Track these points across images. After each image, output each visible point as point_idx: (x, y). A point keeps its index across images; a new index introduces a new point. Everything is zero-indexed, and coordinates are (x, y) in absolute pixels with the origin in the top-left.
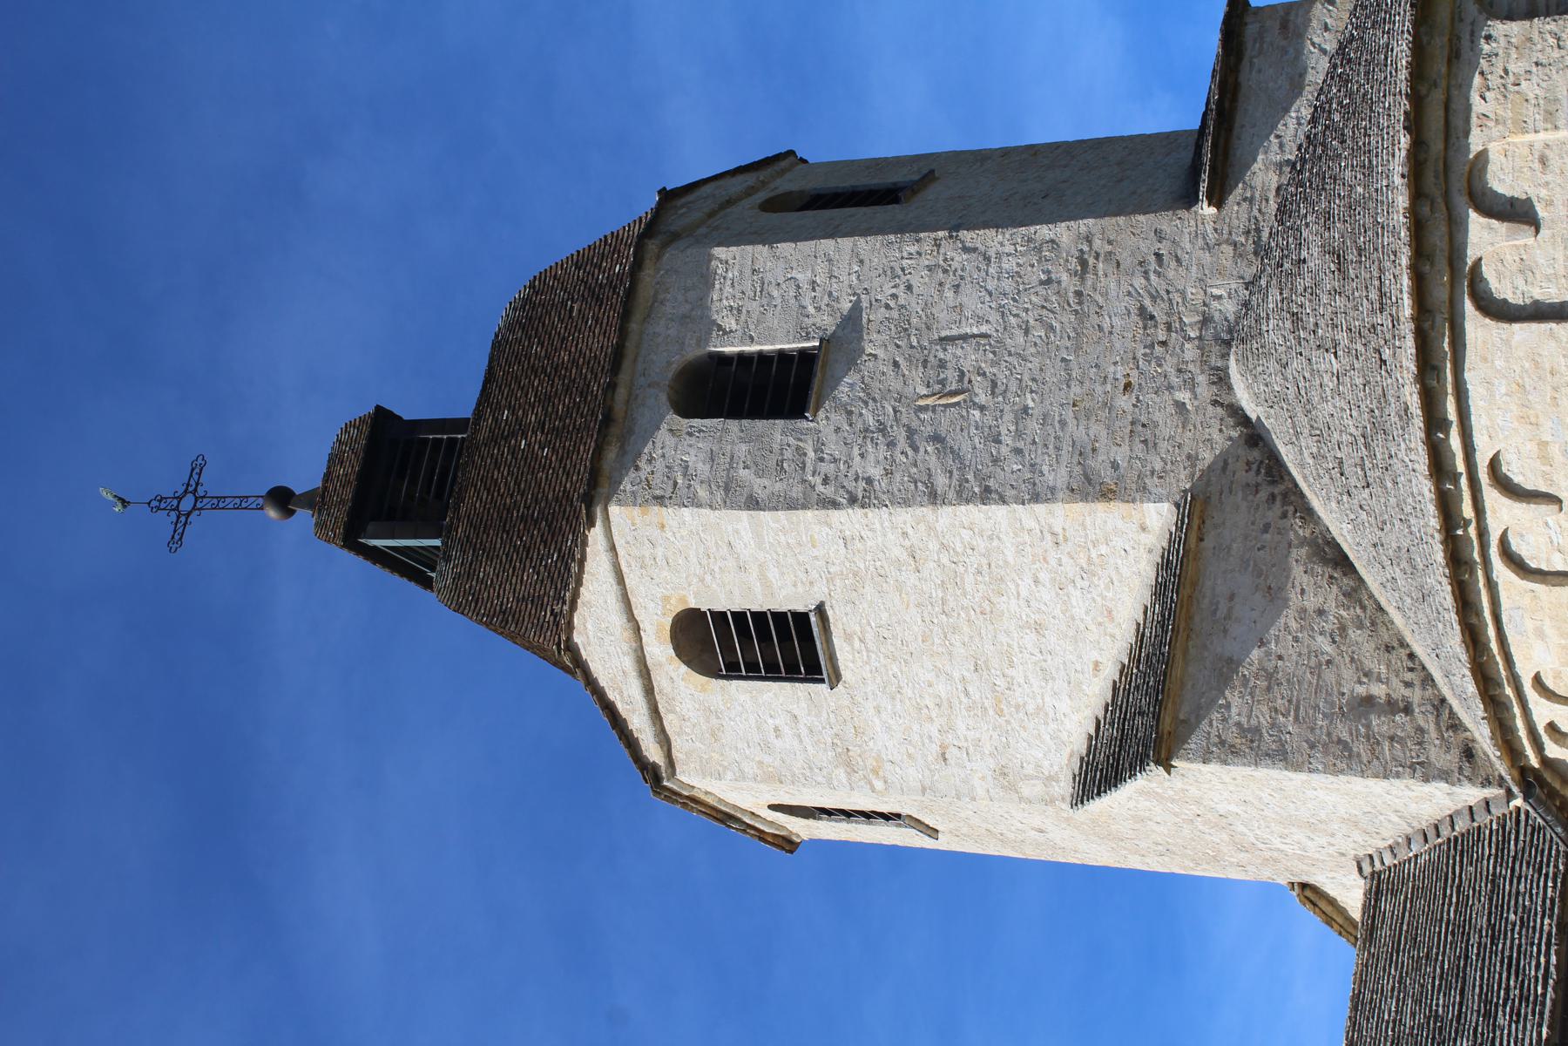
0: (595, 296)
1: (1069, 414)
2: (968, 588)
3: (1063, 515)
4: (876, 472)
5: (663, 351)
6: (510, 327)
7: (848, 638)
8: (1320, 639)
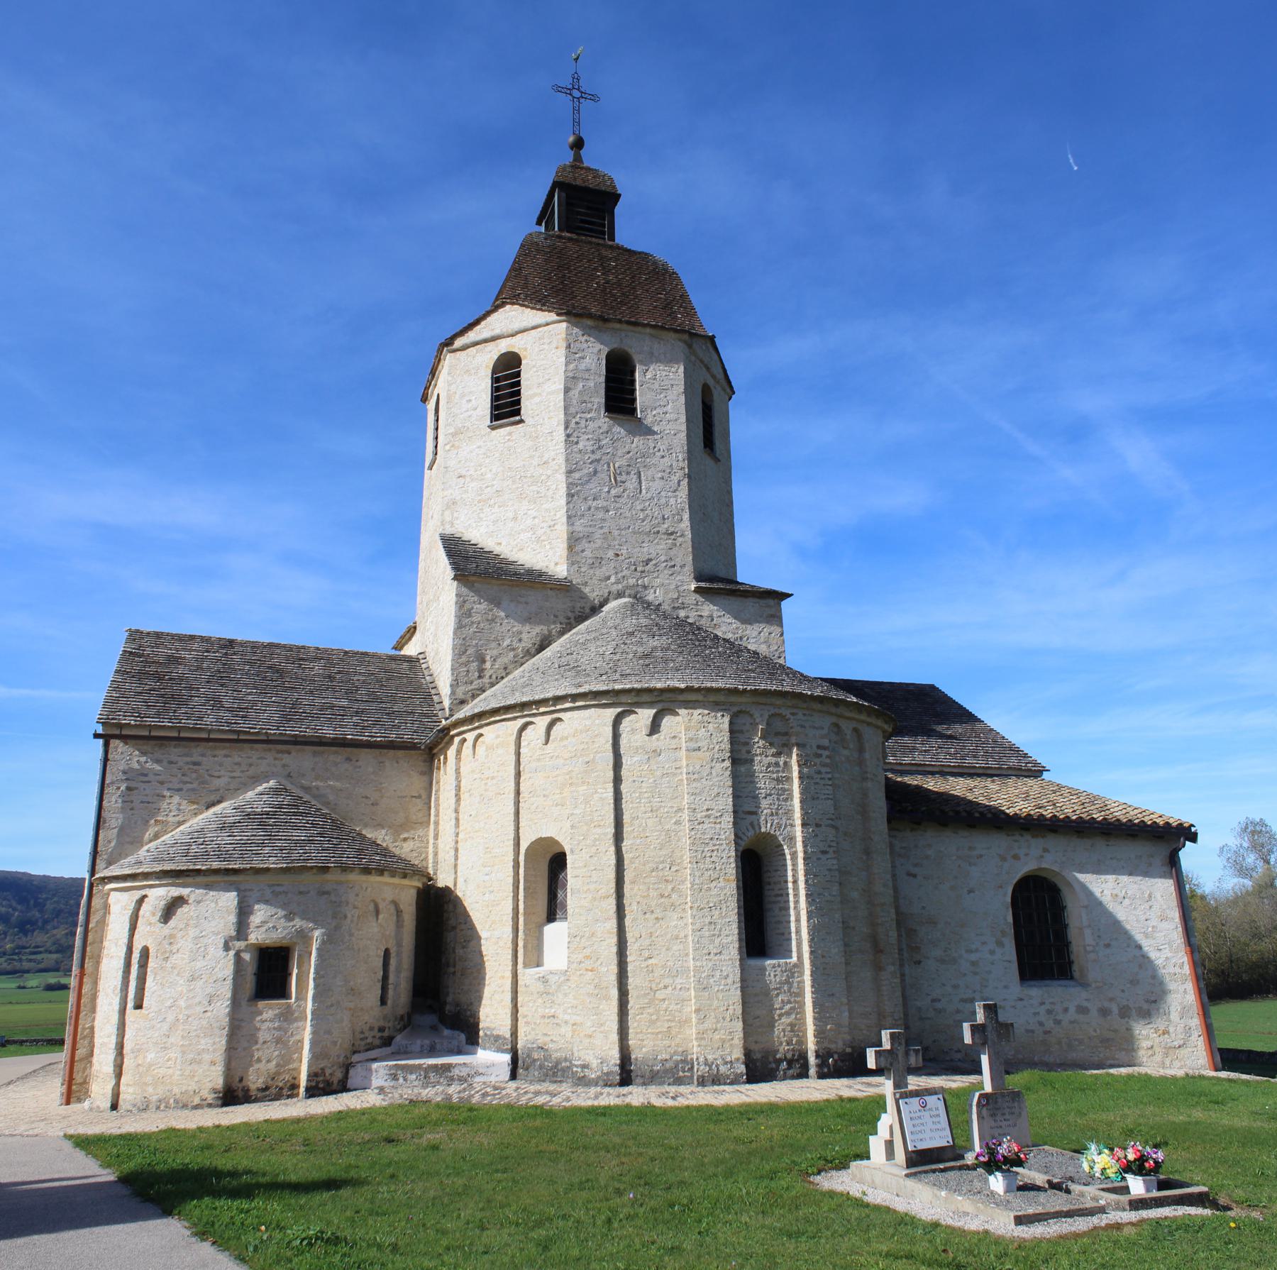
0: (667, 306)
1: (606, 530)
3: (562, 529)
4: (581, 446)
5: (635, 344)
6: (655, 263)
7: (510, 434)
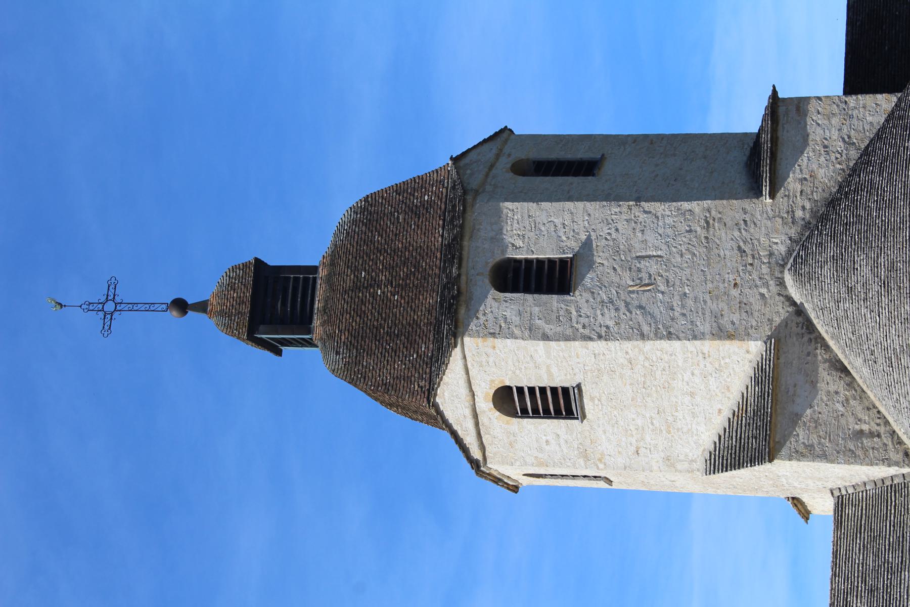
1: (707, 297)
2: (657, 377)
3: (708, 346)
4: (611, 323)
5: (479, 260)
6: (354, 222)
7: (592, 399)
8: (837, 405)
